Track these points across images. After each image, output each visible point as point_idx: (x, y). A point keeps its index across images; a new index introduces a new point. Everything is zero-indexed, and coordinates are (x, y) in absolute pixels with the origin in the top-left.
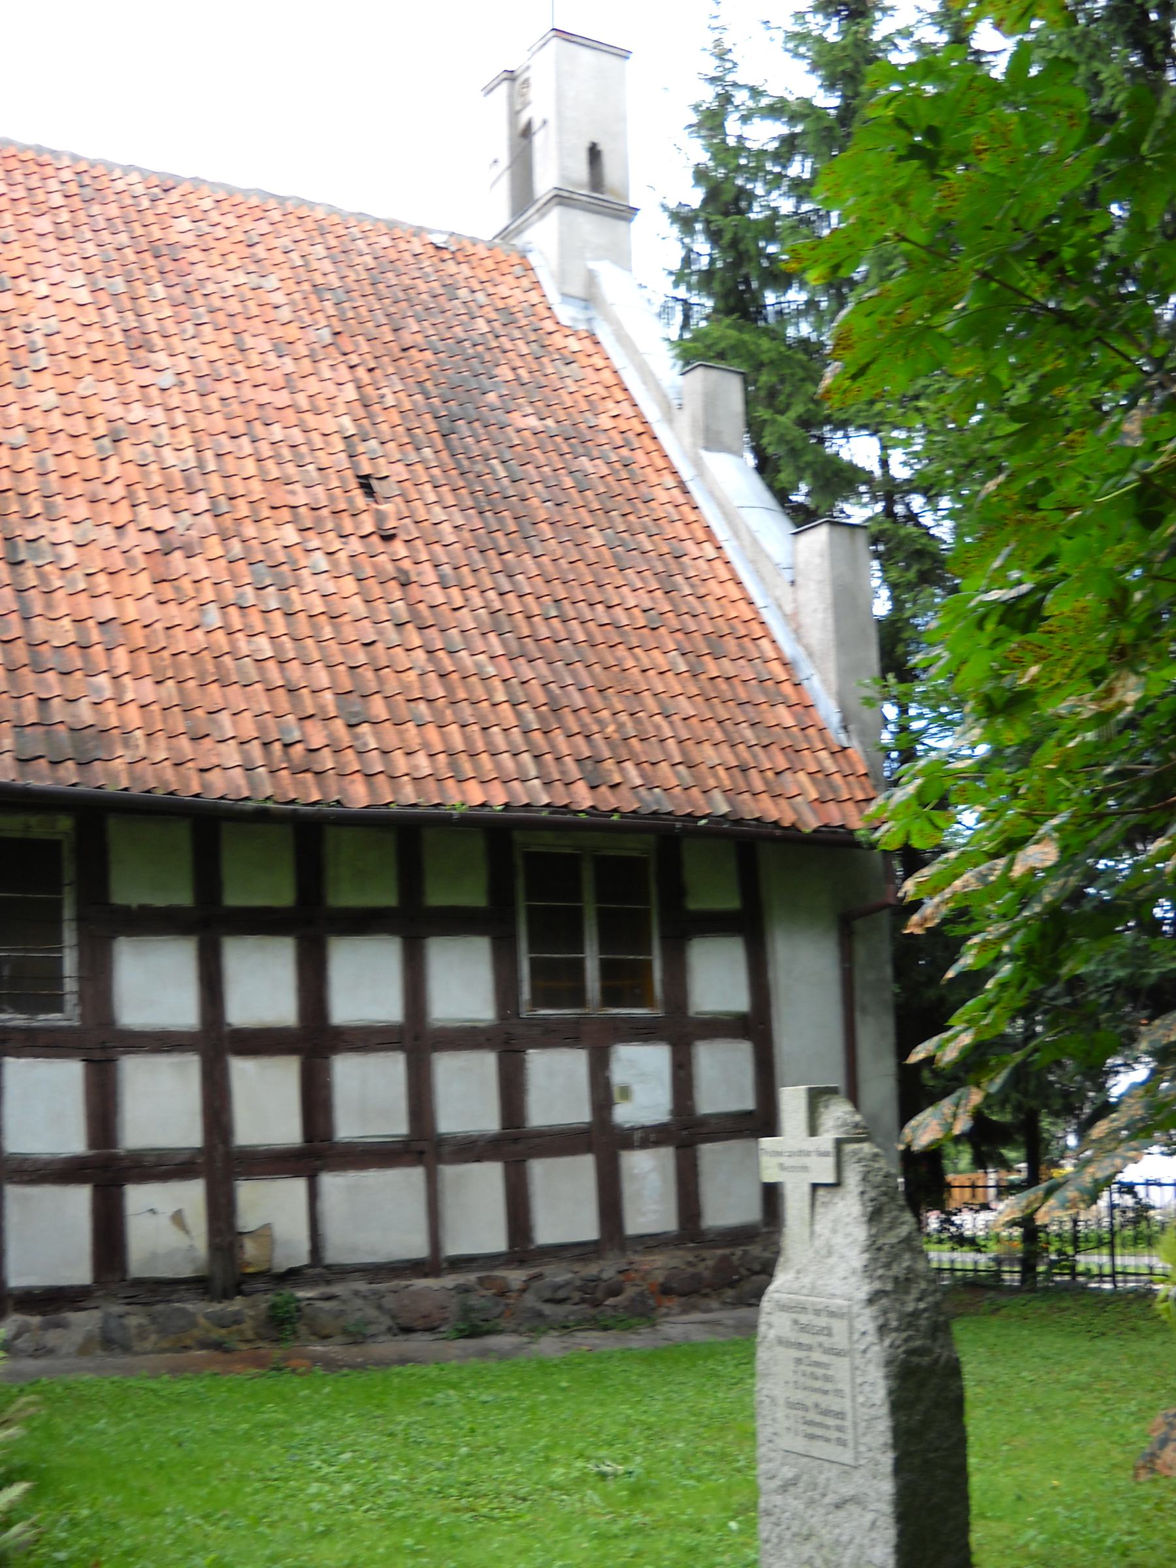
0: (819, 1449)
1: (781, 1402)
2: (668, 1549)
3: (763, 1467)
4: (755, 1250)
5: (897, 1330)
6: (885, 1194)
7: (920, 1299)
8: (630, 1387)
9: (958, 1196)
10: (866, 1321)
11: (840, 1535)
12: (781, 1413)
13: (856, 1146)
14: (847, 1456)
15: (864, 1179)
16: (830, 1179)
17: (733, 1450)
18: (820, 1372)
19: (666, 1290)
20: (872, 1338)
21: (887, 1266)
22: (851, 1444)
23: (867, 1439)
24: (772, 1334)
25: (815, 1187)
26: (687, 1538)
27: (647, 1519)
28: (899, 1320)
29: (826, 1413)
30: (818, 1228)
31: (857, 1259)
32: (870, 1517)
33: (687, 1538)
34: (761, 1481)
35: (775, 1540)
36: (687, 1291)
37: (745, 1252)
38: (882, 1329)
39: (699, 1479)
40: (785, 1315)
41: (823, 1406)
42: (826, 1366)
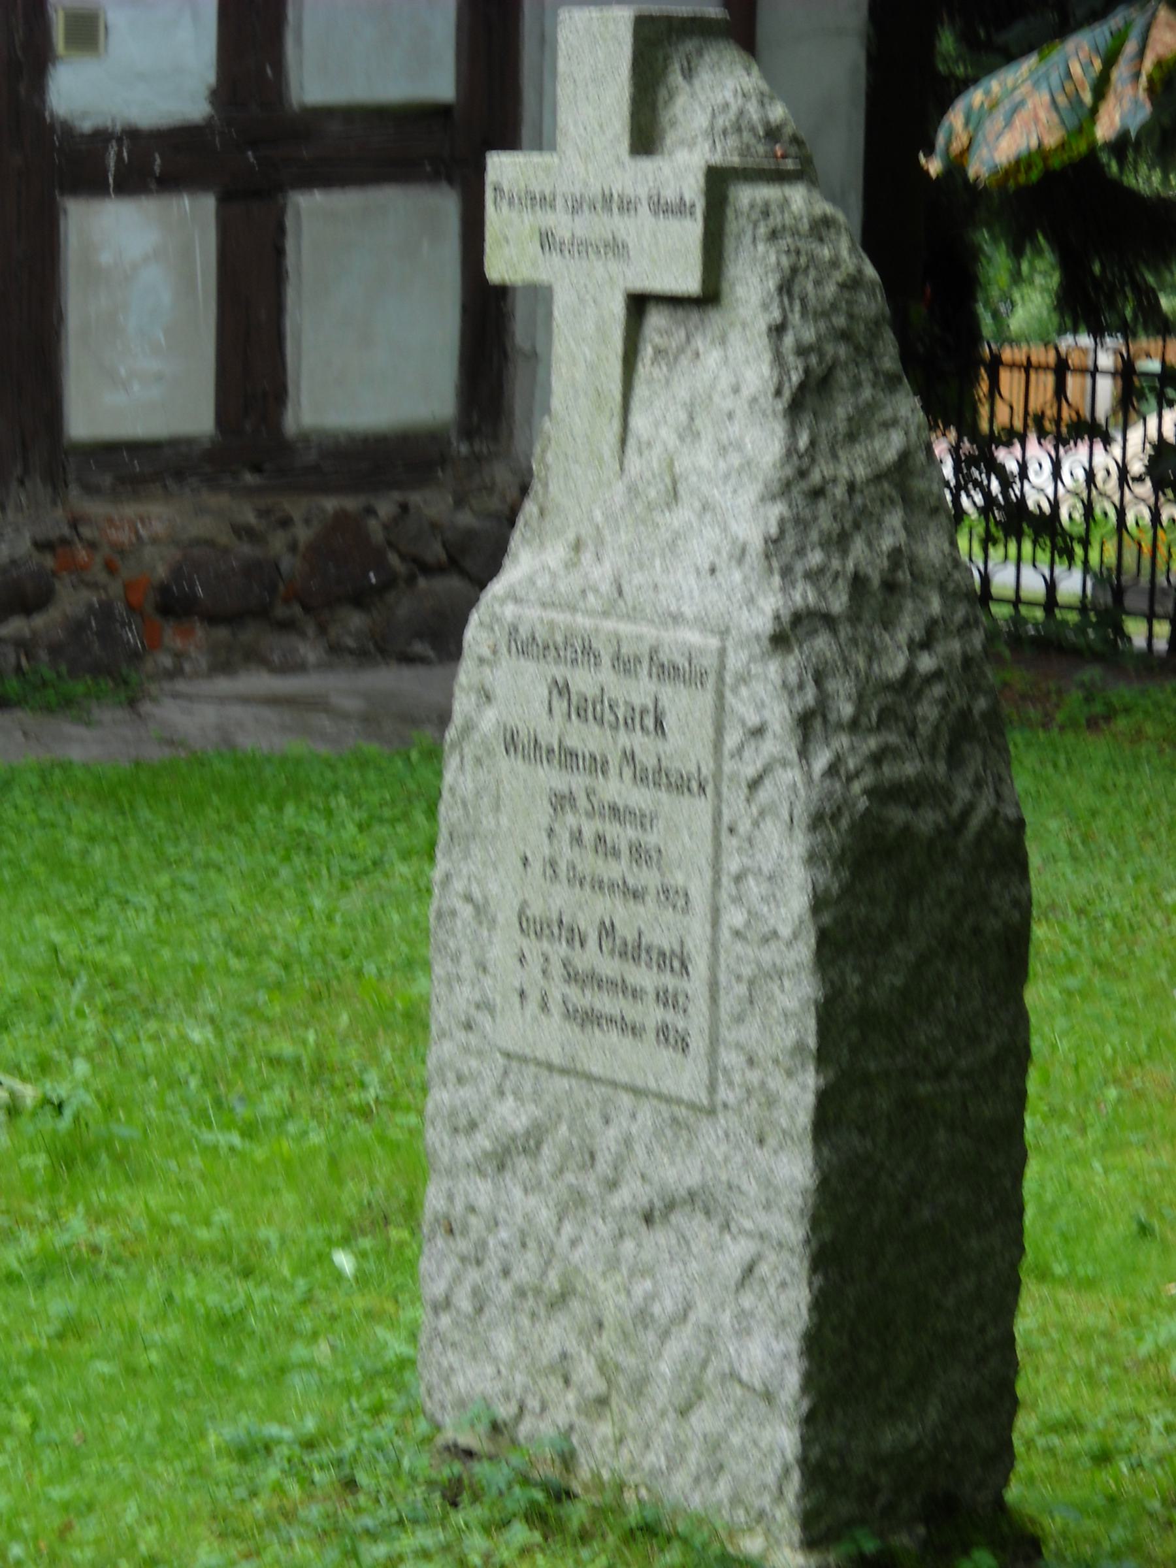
0: (605, 1053)
1: (506, 915)
2: (159, 1319)
3: (441, 1097)
4: (433, 504)
5: (854, 726)
6: (844, 336)
7: (926, 644)
8: (60, 867)
9: (1012, 396)
10: (765, 696)
11: (651, 1297)
12: (501, 947)
13: (767, 192)
14: (685, 1078)
15: (786, 288)
16: (690, 283)
17: (353, 1053)
18: (621, 834)
19: (173, 604)
20: (779, 742)
21: (839, 542)
22: (698, 1043)
23: (750, 1032)
24: (488, 721)
25: (639, 304)
26: (210, 1291)
27: (103, 1234)
28: (860, 701)
29: (634, 952)
30: (639, 422)
31: (750, 518)
32: (738, 1250)
33: (210, 1291)
34: (435, 1136)
35: (464, 1304)
36: (234, 610)
37: (404, 508)
38: (808, 724)
39: (249, 1131)
40: (530, 667)
41: (626, 932)
42: (643, 820)
